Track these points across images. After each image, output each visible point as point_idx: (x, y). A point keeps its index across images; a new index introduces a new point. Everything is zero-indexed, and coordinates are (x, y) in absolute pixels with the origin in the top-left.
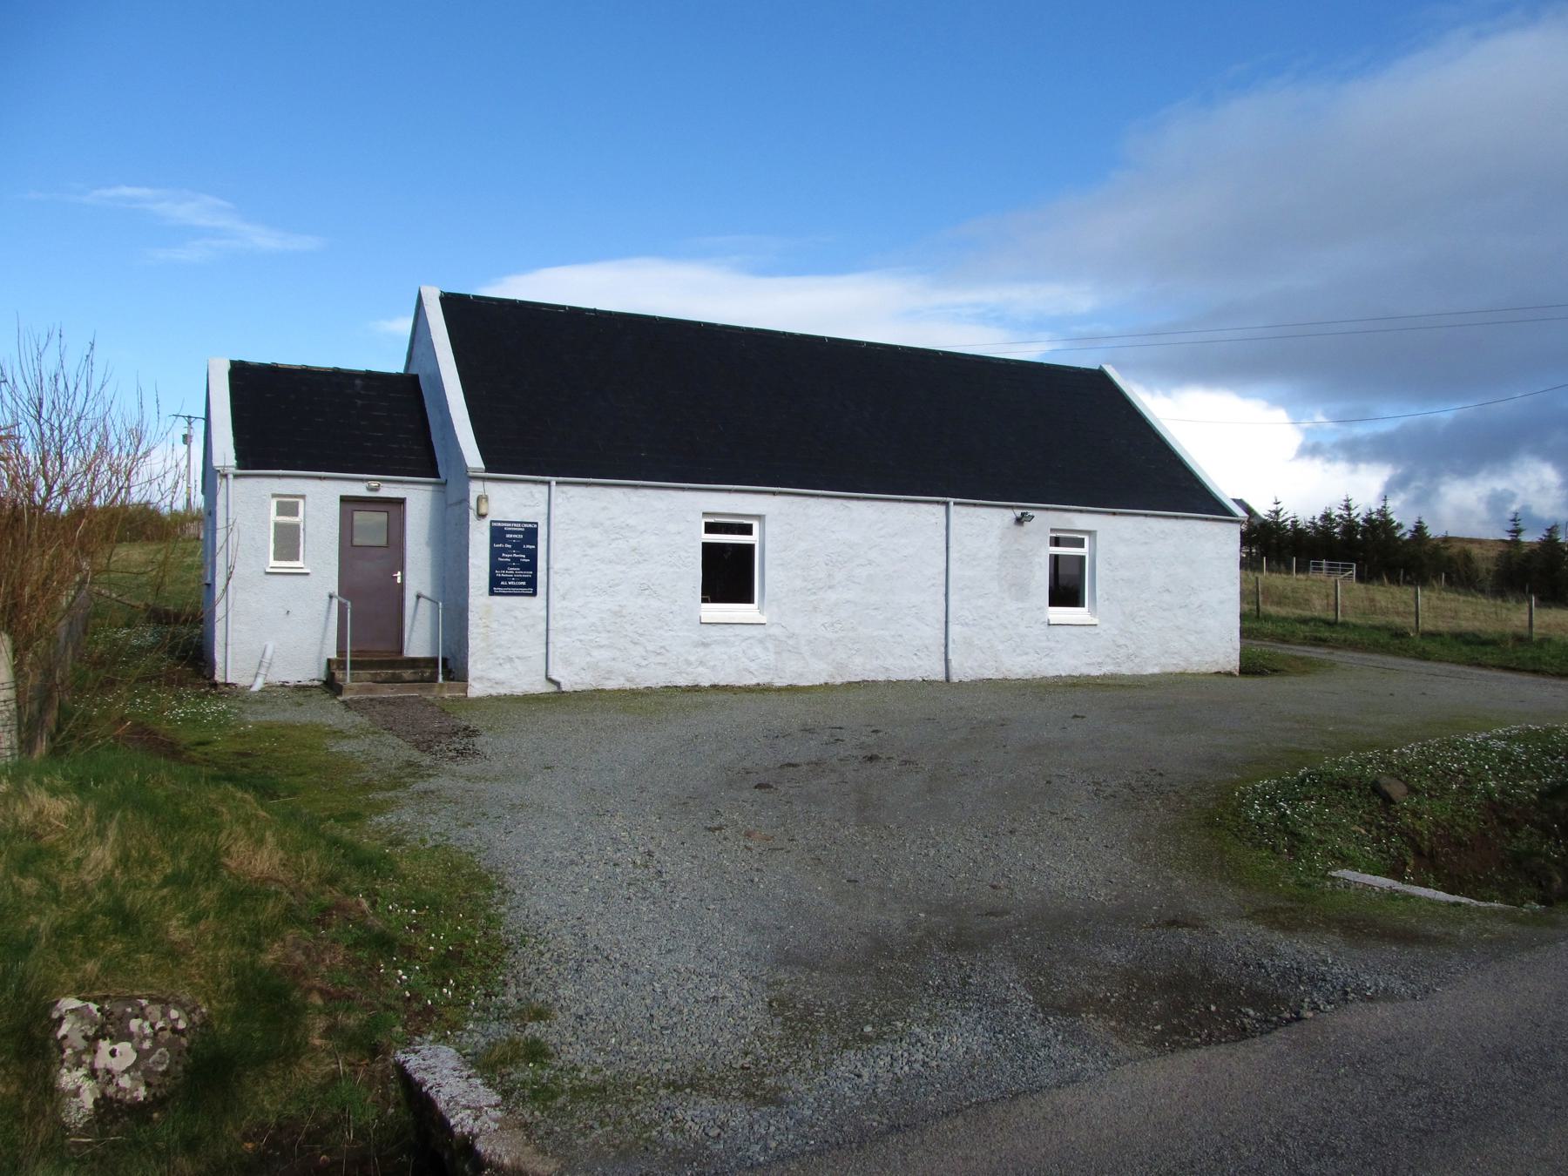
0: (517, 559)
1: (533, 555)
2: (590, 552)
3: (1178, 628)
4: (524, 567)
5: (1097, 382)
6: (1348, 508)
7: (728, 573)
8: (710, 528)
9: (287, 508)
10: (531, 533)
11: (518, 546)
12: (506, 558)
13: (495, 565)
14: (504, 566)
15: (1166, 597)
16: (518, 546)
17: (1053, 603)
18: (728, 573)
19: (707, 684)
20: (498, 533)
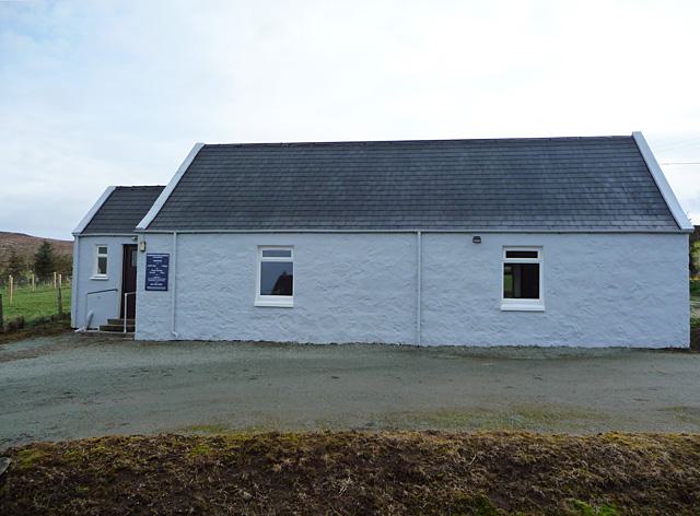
0: (160, 273)
1: (166, 270)
2: (196, 268)
3: (624, 314)
4: (162, 276)
5: (207, 154)
6: (477, 240)
7: (523, 281)
8: (509, 255)
9: (103, 250)
10: (166, 260)
11: (159, 266)
12: (153, 271)
13: (148, 275)
14: (152, 276)
15: (611, 291)
16: (159, 266)
17: (538, 297)
18: (523, 281)
19: (258, 340)
20: (150, 260)
